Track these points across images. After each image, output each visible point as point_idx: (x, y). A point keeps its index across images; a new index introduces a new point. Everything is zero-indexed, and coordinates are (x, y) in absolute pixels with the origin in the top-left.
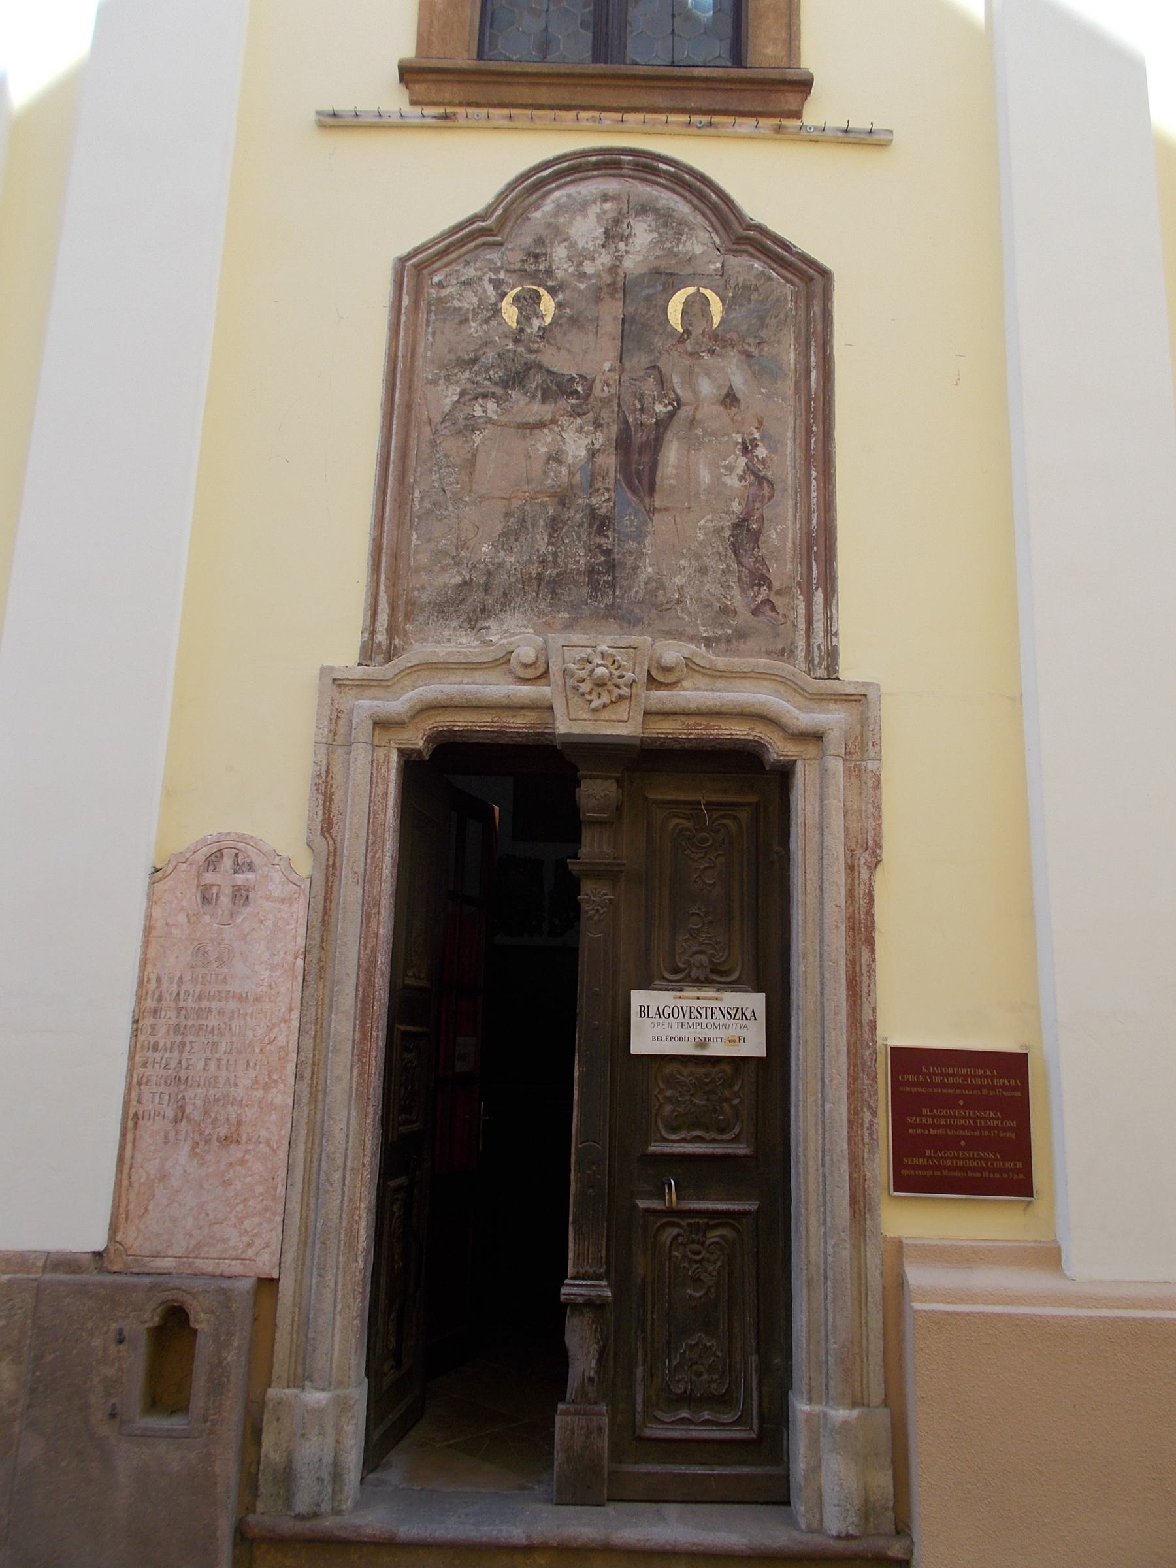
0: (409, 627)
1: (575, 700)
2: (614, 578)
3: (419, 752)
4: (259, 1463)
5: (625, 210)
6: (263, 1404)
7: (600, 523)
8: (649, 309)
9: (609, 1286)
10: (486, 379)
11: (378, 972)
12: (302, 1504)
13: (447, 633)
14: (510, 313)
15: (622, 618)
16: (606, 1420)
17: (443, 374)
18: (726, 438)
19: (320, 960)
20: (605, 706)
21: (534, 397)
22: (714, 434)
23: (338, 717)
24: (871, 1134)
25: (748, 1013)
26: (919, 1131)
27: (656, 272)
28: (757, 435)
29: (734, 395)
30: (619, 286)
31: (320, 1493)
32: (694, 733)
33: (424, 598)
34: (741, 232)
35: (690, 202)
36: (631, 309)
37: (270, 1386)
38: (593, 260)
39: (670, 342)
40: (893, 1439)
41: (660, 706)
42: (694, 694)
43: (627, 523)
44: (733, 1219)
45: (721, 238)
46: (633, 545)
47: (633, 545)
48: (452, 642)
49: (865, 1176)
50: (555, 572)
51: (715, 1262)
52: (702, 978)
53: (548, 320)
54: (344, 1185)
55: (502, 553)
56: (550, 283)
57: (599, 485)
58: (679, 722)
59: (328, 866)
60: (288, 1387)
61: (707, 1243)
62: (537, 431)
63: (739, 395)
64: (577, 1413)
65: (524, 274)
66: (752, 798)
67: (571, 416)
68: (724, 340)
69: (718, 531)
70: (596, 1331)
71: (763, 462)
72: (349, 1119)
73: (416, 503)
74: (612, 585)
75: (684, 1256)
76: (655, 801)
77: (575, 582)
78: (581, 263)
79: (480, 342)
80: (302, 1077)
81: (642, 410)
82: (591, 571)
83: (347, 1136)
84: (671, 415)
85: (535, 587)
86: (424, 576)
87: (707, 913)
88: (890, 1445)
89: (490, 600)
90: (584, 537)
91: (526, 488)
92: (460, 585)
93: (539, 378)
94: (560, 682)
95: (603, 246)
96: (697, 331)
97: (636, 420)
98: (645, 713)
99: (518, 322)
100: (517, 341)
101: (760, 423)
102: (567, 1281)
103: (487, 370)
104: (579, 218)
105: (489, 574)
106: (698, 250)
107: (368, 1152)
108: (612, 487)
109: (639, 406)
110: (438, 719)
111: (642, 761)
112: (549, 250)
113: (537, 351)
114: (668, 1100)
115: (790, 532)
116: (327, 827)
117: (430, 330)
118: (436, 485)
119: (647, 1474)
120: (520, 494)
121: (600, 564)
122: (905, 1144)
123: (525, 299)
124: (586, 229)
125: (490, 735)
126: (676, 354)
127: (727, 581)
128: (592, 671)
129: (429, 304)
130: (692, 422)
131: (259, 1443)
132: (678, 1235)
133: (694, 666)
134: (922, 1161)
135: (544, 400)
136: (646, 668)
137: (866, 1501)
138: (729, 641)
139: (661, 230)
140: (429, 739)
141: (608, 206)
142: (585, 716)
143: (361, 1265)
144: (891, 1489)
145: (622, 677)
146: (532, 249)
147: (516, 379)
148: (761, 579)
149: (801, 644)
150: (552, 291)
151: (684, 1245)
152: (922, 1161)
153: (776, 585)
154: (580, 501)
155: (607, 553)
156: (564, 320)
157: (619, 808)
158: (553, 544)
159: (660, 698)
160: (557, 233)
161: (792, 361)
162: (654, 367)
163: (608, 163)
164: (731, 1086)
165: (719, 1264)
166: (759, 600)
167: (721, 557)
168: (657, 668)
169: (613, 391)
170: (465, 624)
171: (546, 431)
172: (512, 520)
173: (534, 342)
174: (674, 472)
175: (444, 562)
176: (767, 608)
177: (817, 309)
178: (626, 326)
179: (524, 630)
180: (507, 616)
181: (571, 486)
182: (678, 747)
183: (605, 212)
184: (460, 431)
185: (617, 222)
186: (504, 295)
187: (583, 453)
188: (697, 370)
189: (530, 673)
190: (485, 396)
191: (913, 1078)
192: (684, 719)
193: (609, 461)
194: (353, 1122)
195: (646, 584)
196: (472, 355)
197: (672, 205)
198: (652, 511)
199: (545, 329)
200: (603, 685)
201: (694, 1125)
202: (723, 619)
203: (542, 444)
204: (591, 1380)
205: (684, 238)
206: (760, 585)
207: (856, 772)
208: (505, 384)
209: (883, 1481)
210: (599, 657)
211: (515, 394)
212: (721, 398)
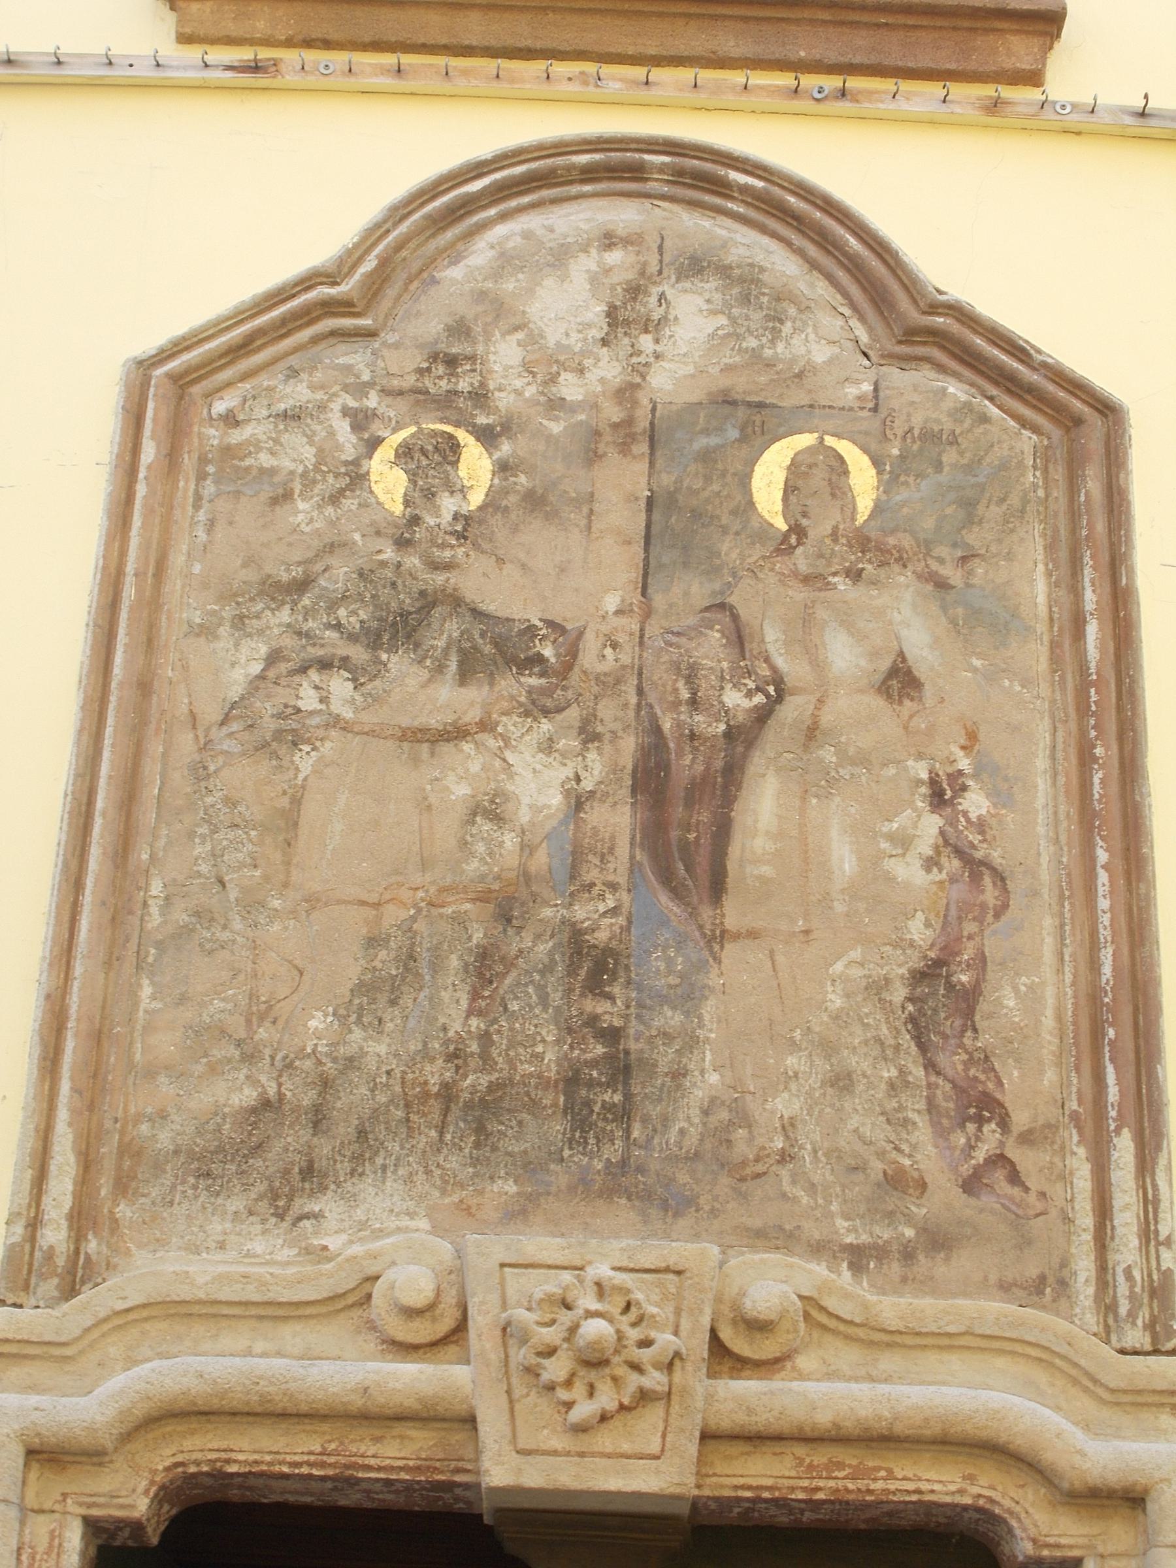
0: (124, 1211)
1: (531, 1402)
2: (628, 1096)
3: (137, 1527)
5: (653, 268)
7: (594, 965)
8: (708, 479)
10: (329, 626)
13: (217, 1227)
14: (389, 483)
15: (647, 1196)
17: (228, 612)
18: (892, 771)
20: (604, 1418)
21: (440, 669)
22: (862, 760)
27: (726, 401)
28: (964, 764)
29: (909, 672)
30: (641, 430)
32: (826, 1487)
33: (165, 1139)
34: (916, 318)
35: (800, 253)
36: (666, 480)
38: (581, 371)
39: (757, 552)
41: (741, 1418)
42: (824, 1389)
43: (659, 966)
45: (870, 330)
46: (671, 1018)
47: (671, 1018)
48: (223, 1249)
50: (485, 1080)
53: (476, 499)
55: (357, 1034)
56: (482, 420)
57: (591, 874)
58: (789, 1461)
62: (446, 748)
63: (921, 672)
65: (421, 398)
67: (527, 714)
68: (881, 549)
69: (877, 988)
71: (981, 826)
73: (154, 910)
74: (624, 1114)
77: (534, 1106)
78: (553, 379)
79: (316, 544)
81: (694, 702)
82: (572, 1080)
84: (763, 716)
85: (436, 1117)
86: (165, 1086)
89: (324, 1148)
90: (556, 998)
91: (417, 879)
92: (254, 1110)
93: (453, 628)
94: (495, 1356)
95: (605, 342)
96: (819, 530)
97: (679, 725)
98: (707, 1437)
99: (407, 503)
100: (403, 543)
101: (972, 736)
103: (333, 606)
104: (549, 282)
105: (325, 1083)
106: (820, 354)
108: (622, 880)
109: (685, 695)
110: (188, 1444)
112: (480, 349)
113: (448, 566)
115: (1050, 994)
117: (202, 516)
118: (204, 868)
120: (405, 894)
121: (594, 1063)
123: (423, 452)
124: (565, 306)
126: (772, 579)
127: (901, 1108)
128: (573, 1329)
129: (203, 460)
130: (812, 733)
133: (823, 1319)
135: (464, 677)
136: (706, 1321)
138: (908, 1255)
139: (736, 311)
140: (164, 1494)
141: (615, 257)
142: (556, 1443)
145: (646, 1343)
146: (442, 346)
147: (399, 628)
148: (982, 1107)
149: (1084, 1266)
150: (487, 437)
153: (1020, 1119)
154: (547, 912)
155: (612, 1036)
156: (513, 499)
158: (480, 1013)
159: (743, 1397)
160: (500, 312)
161: (1041, 599)
162: (722, 606)
163: (616, 167)
166: (980, 1155)
167: (885, 1051)
168: (734, 1322)
169: (626, 659)
170: (263, 1206)
171: (467, 747)
172: (383, 954)
173: (444, 546)
174: (770, 847)
175: (217, 1053)
176: (999, 1176)
177: (1093, 485)
178: (656, 516)
179: (405, 1222)
180: (366, 1187)
181: (526, 877)
182: (784, 1519)
183: (608, 271)
184: (265, 745)
185: (635, 291)
186: (374, 443)
187: (555, 800)
188: (821, 613)
189: (421, 1331)
190: (325, 665)
192: (800, 1450)
193: (617, 820)
195: (706, 1113)
196: (297, 572)
197: (760, 258)
198: (718, 937)
199: (468, 519)
202: (892, 1201)
203: (460, 776)
205: (787, 328)
206: (980, 1121)
208: (373, 638)
210: (592, 1291)
211: (397, 662)
212: (879, 677)
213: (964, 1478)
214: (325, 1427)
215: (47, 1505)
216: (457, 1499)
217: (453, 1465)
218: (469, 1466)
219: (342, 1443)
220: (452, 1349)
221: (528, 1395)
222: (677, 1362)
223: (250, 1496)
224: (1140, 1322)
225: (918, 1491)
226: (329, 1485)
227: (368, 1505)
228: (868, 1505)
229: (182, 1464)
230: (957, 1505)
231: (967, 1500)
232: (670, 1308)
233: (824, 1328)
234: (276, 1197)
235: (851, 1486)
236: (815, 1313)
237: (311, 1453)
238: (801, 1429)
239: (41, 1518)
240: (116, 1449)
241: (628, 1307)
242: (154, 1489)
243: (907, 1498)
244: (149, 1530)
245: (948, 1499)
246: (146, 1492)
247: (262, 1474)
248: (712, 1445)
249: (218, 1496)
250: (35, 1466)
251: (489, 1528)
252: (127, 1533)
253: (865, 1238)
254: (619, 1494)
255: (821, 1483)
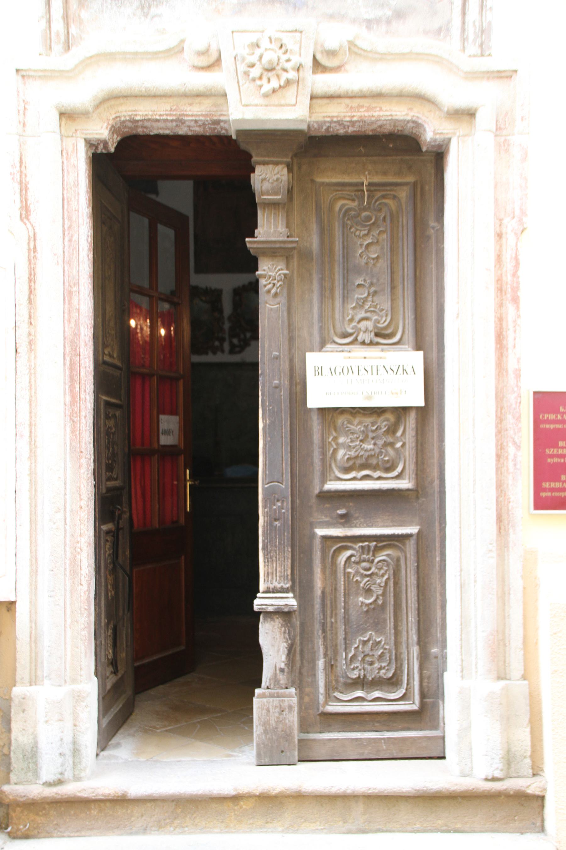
0: (84, 14)
1: (247, 86)
3: (105, 143)
4: (10, 744)
6: (10, 700)
9: (294, 597)
11: (82, 344)
12: (48, 772)
16: (295, 700)
19: (30, 334)
20: (274, 91)
23: (25, 108)
24: (515, 465)
25: (409, 370)
26: (556, 460)
31: (62, 765)
32: (357, 116)
37: (15, 686)
40: (530, 705)
42: (356, 78)
44: (397, 541)
49: (509, 498)
51: (383, 576)
52: (367, 341)
54: (66, 524)
59: (29, 250)
60: (31, 685)
61: (376, 560)
64: (272, 696)
66: (410, 179)
70: (285, 633)
72: (65, 469)
75: (357, 573)
76: (323, 184)
80: (21, 436)
83: (65, 483)
87: (372, 284)
88: (528, 708)
98: (312, 98)
102: (258, 595)
107: (84, 496)
110: (120, 109)
111: (310, 148)
114: (343, 445)
116: (25, 213)
119: (330, 740)
122: (543, 471)
125: (169, 125)
128: (261, 57)
131: (9, 730)
132: (352, 556)
133: (356, 50)
134: (558, 485)
137: (508, 751)
140: (114, 130)
143: (85, 587)
144: (529, 743)
145: (288, 60)
151: (357, 563)
152: (558, 485)
157: (290, 191)
159: (325, 82)
164: (394, 432)
165: (386, 577)
168: (322, 53)
182: (342, 132)
189: (203, 61)
191: (552, 417)
192: (347, 101)
194: (69, 471)
200: (273, 69)
201: (364, 466)
204: (282, 670)
207: (503, 147)
209: (523, 737)
213: (408, 109)
214: (171, 100)
215: (70, 134)
216: (222, 128)
217: (219, 113)
218: (225, 113)
219: (177, 106)
220: (216, 68)
221: (245, 83)
222: (301, 69)
223: (147, 132)
224: (477, 44)
225: (391, 115)
226: (174, 124)
227: (190, 133)
228: (372, 123)
229: (119, 117)
230: (405, 121)
231: (409, 118)
232: (298, 46)
233: (356, 54)
234: (143, 8)
235: (366, 114)
236: (352, 48)
237: (166, 111)
238: (347, 93)
239: (69, 139)
240: (93, 112)
241: (281, 46)
242: (109, 127)
243: (387, 118)
244: (110, 144)
245: (402, 118)
246: (107, 128)
247: (149, 120)
248: (314, 101)
249: (134, 132)
250: (64, 119)
251: (235, 141)
252: (101, 146)
253: (371, 16)
254: (281, 120)
255: (355, 114)
